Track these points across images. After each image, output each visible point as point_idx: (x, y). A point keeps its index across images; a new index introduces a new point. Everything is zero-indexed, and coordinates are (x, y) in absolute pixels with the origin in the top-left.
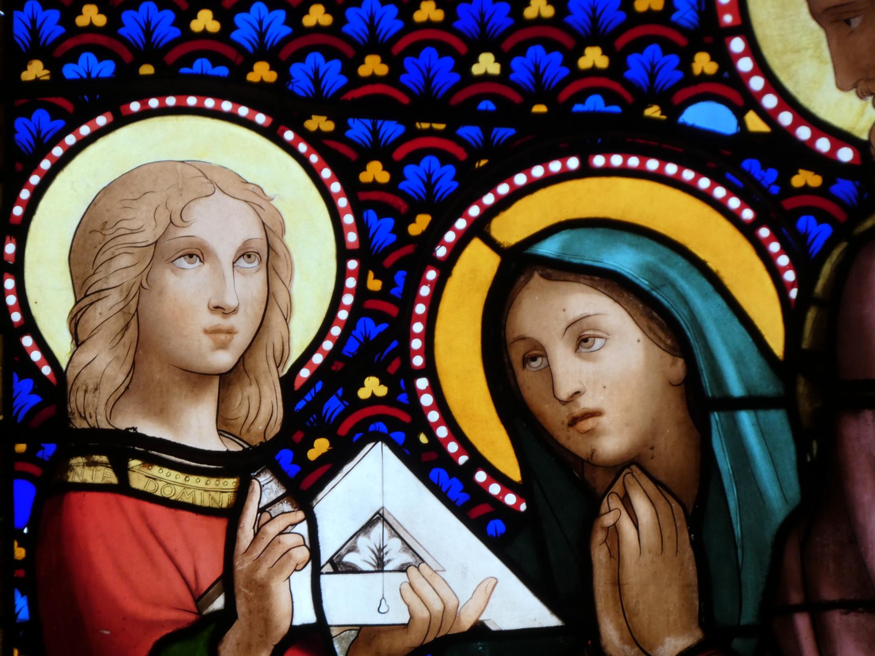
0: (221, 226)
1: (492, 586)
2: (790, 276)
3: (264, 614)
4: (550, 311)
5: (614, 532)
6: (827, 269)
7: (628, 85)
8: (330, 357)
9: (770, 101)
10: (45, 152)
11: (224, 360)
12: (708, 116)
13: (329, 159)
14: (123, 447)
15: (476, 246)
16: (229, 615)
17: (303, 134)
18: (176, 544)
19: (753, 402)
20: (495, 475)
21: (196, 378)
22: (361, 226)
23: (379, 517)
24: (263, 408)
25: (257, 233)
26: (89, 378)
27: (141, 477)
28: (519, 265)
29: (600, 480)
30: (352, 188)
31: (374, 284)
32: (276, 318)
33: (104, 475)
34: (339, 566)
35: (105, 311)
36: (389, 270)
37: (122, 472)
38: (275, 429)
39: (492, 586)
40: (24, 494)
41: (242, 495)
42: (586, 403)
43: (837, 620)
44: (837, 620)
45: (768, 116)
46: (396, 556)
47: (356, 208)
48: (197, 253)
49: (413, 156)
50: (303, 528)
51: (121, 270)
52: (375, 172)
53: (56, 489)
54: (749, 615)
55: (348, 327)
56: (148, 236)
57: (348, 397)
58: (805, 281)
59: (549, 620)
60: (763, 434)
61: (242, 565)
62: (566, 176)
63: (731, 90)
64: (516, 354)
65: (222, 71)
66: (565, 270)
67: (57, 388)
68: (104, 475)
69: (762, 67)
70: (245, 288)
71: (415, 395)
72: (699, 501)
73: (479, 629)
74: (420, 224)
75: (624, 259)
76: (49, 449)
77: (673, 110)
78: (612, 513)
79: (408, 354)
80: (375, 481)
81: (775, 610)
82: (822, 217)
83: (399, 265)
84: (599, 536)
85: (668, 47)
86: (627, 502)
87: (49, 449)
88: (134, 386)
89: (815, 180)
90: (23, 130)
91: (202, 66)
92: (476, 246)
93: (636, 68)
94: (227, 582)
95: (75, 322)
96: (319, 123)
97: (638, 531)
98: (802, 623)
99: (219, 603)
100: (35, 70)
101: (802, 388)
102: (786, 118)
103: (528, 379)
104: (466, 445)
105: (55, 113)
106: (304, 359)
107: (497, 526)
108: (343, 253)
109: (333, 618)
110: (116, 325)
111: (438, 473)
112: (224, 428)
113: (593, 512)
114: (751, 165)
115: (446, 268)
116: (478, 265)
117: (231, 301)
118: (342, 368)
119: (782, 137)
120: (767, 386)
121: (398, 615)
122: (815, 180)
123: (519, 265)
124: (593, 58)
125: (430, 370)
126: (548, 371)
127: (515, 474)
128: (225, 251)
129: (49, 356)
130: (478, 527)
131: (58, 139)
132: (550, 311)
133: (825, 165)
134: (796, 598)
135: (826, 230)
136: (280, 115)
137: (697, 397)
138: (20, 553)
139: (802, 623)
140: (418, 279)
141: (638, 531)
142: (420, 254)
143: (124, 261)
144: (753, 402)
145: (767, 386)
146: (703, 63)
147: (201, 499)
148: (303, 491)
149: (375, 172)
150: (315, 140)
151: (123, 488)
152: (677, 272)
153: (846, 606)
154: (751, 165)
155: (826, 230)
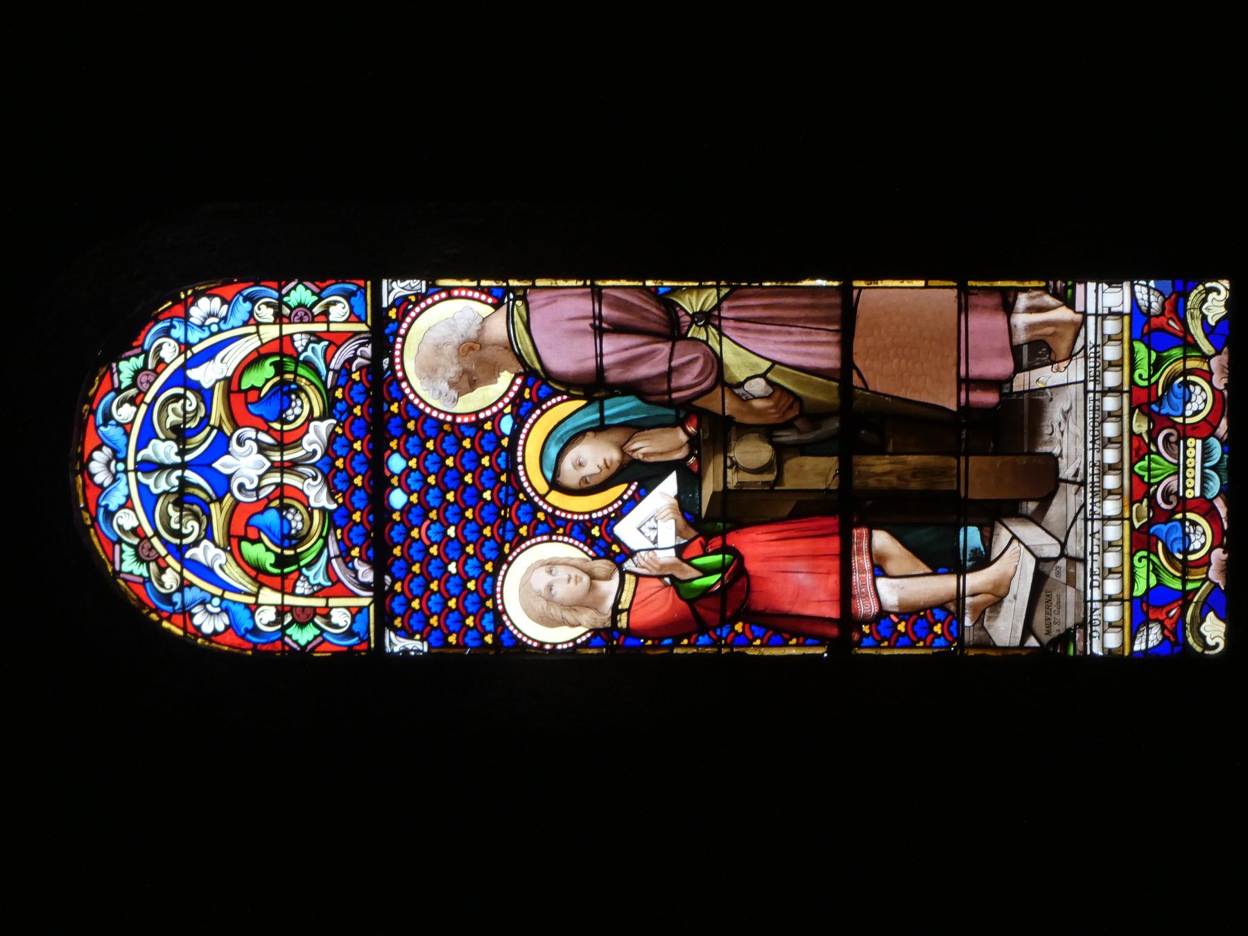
0: (541, 580)
1: (664, 495)
2: (559, 399)
3: (672, 565)
4: (570, 475)
5: (645, 455)
6: (557, 387)
7: (495, 450)
8: (585, 544)
9: (501, 405)
10: (515, 636)
11: (586, 579)
12: (506, 425)
13: (518, 545)
14: (616, 611)
15: (547, 498)
16: (672, 577)
17: (510, 553)
18: (647, 593)
19: (601, 410)
20: (625, 492)
21: (592, 587)
22: (542, 535)
23: (639, 529)
24: (602, 566)
25: (543, 568)
26: (592, 622)
27: (624, 604)
28: (554, 485)
29: (627, 459)
30: (528, 538)
31: (561, 531)
32: (572, 562)
33: (624, 616)
34: (655, 542)
35: (569, 616)
36: (555, 526)
37: (623, 611)
38: (609, 562)
39: (664, 495)
40: (630, 642)
41: (631, 573)
42: (601, 463)
43: (673, 385)
44: (673, 385)
45: (506, 406)
46: (649, 524)
47: (535, 536)
48: (550, 587)
49: (514, 518)
50: (642, 553)
51: (556, 612)
52: (523, 531)
53: (628, 632)
54: (673, 412)
55: (575, 539)
56: (544, 604)
57: (600, 540)
58: (561, 394)
59: (674, 474)
60: (612, 407)
61: (655, 573)
62: (525, 469)
63: (497, 417)
64: (585, 486)
65: (954, 622)
66: (556, 470)
67: (596, 632)
68: (624, 616)
69: (489, 407)
70: (562, 572)
71: (598, 518)
72: (635, 428)
73: (677, 497)
74: (541, 516)
75: (553, 451)
76: (615, 634)
77: (504, 436)
78: (638, 455)
79: (584, 521)
80: (626, 530)
81: (670, 404)
82: (539, 389)
83: (554, 522)
84: (646, 459)
85: (482, 437)
86: (634, 451)
87: (615, 634)
88: (595, 606)
89: (527, 391)
90: (507, 643)
91: (953, 628)
92: (547, 498)
93: (488, 448)
94: (660, 577)
95: (573, 626)
96: (507, 549)
97: (645, 447)
98: (674, 395)
99: (667, 580)
100: (489, 639)
101: (596, 395)
102: (506, 400)
103: (593, 482)
104: (616, 501)
105: (502, 632)
106: (586, 553)
107: (642, 491)
108: (550, 540)
109: (673, 544)
110: (574, 613)
111: (624, 509)
112: (608, 578)
113: (638, 461)
114: (522, 412)
115: (555, 508)
116: (555, 498)
117: (566, 577)
118: (590, 541)
119: (512, 401)
120: (596, 406)
121: (673, 522)
122: (527, 391)
123: (554, 485)
124: (485, 461)
125: (590, 513)
126: (590, 476)
127: (625, 486)
128: (549, 578)
129: (584, 634)
130: (642, 498)
131: (511, 632)
132: (570, 475)
133: (522, 388)
134: (667, 397)
135: (544, 387)
136: (502, 560)
137: (600, 428)
138: (649, 642)
139: (674, 395)
140: (559, 518)
141: (645, 447)
142: (551, 517)
143: (552, 611)
144: (601, 410)
145: (596, 406)
146: (488, 426)
147: (633, 585)
148: (629, 553)
149: (523, 531)
150: (512, 550)
151: (628, 610)
152: (558, 434)
153: (669, 381)
154: (522, 412)
155: (544, 387)
